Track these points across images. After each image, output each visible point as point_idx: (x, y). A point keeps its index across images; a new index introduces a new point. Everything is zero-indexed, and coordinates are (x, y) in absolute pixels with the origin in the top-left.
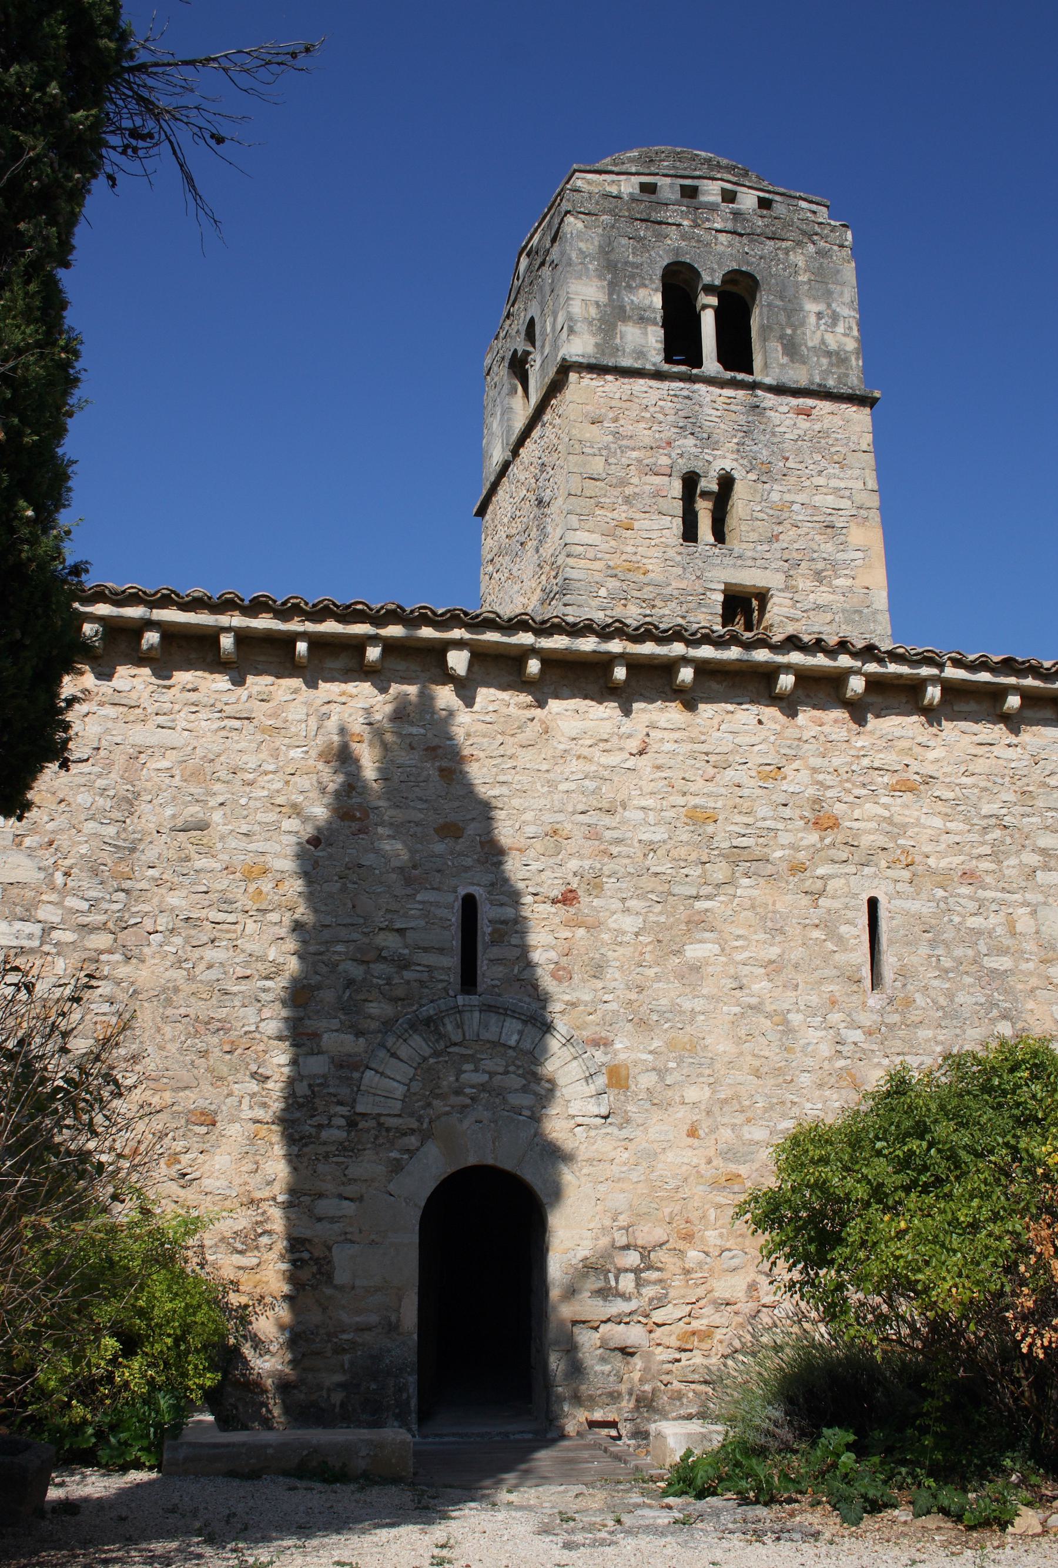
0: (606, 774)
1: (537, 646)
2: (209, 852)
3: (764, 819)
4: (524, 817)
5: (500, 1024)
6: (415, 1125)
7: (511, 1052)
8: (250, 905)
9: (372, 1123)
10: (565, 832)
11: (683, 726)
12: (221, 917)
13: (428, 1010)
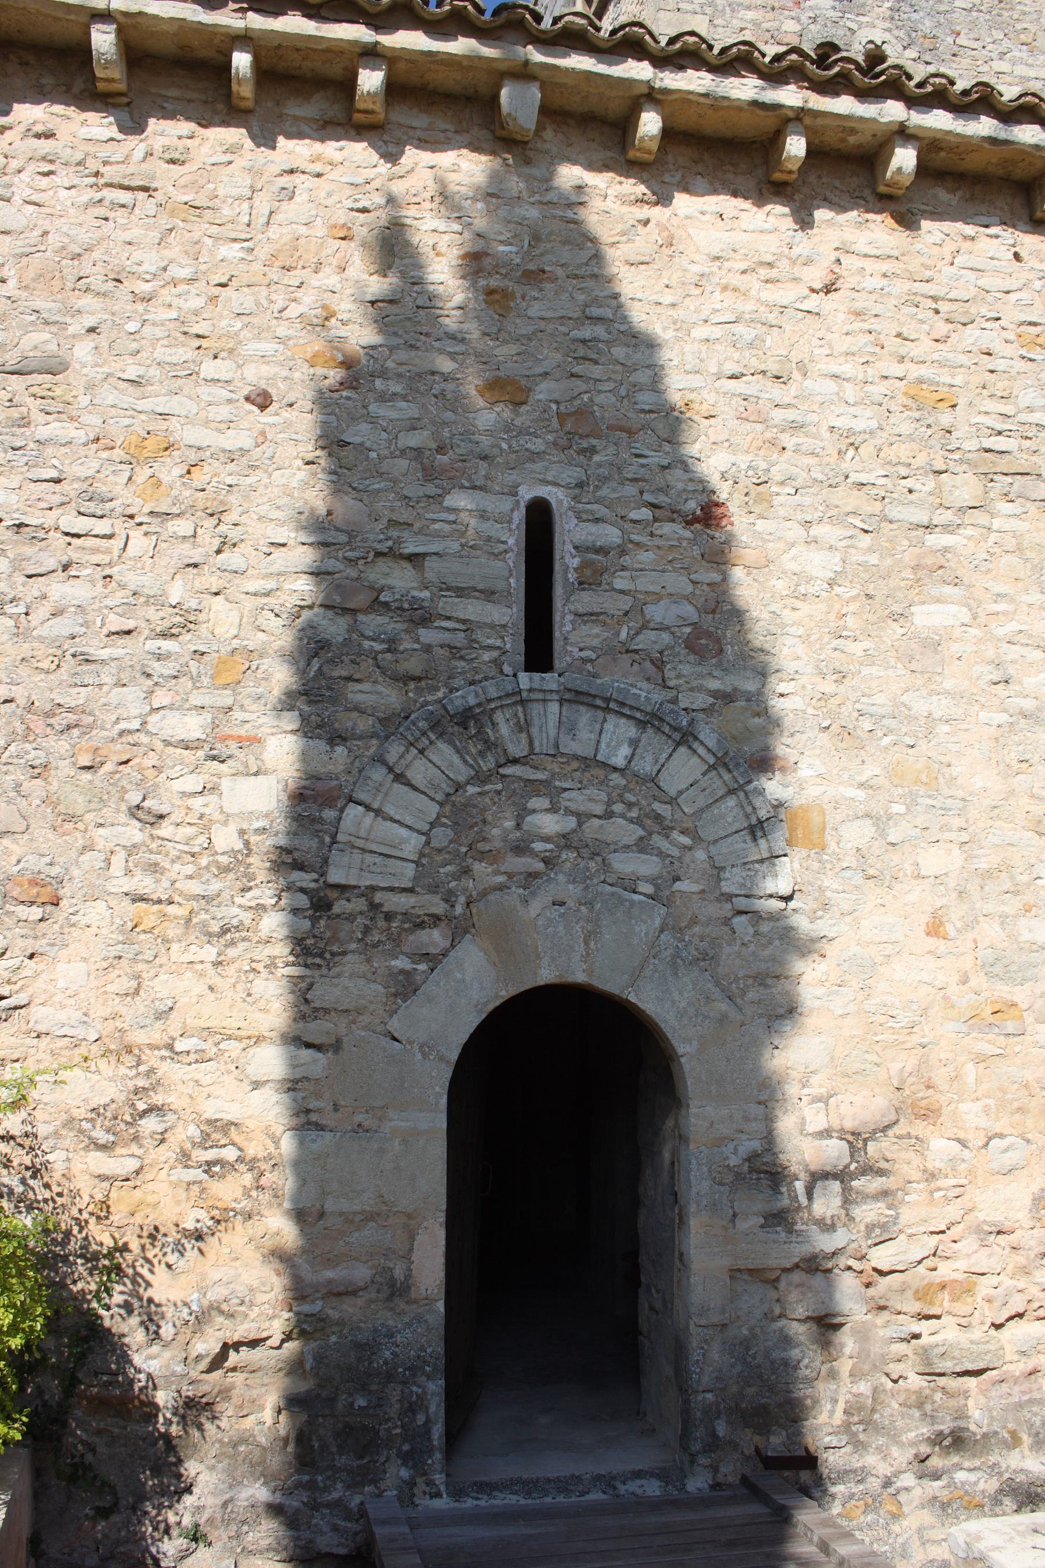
0: (772, 318)
1: (657, 85)
2: (65, 412)
3: (1030, 409)
4: (633, 378)
5: (598, 726)
6: (439, 908)
7: (616, 779)
8: (140, 507)
9: (359, 904)
10: (705, 407)
11: (896, 253)
12: (81, 524)
13: (466, 697)
